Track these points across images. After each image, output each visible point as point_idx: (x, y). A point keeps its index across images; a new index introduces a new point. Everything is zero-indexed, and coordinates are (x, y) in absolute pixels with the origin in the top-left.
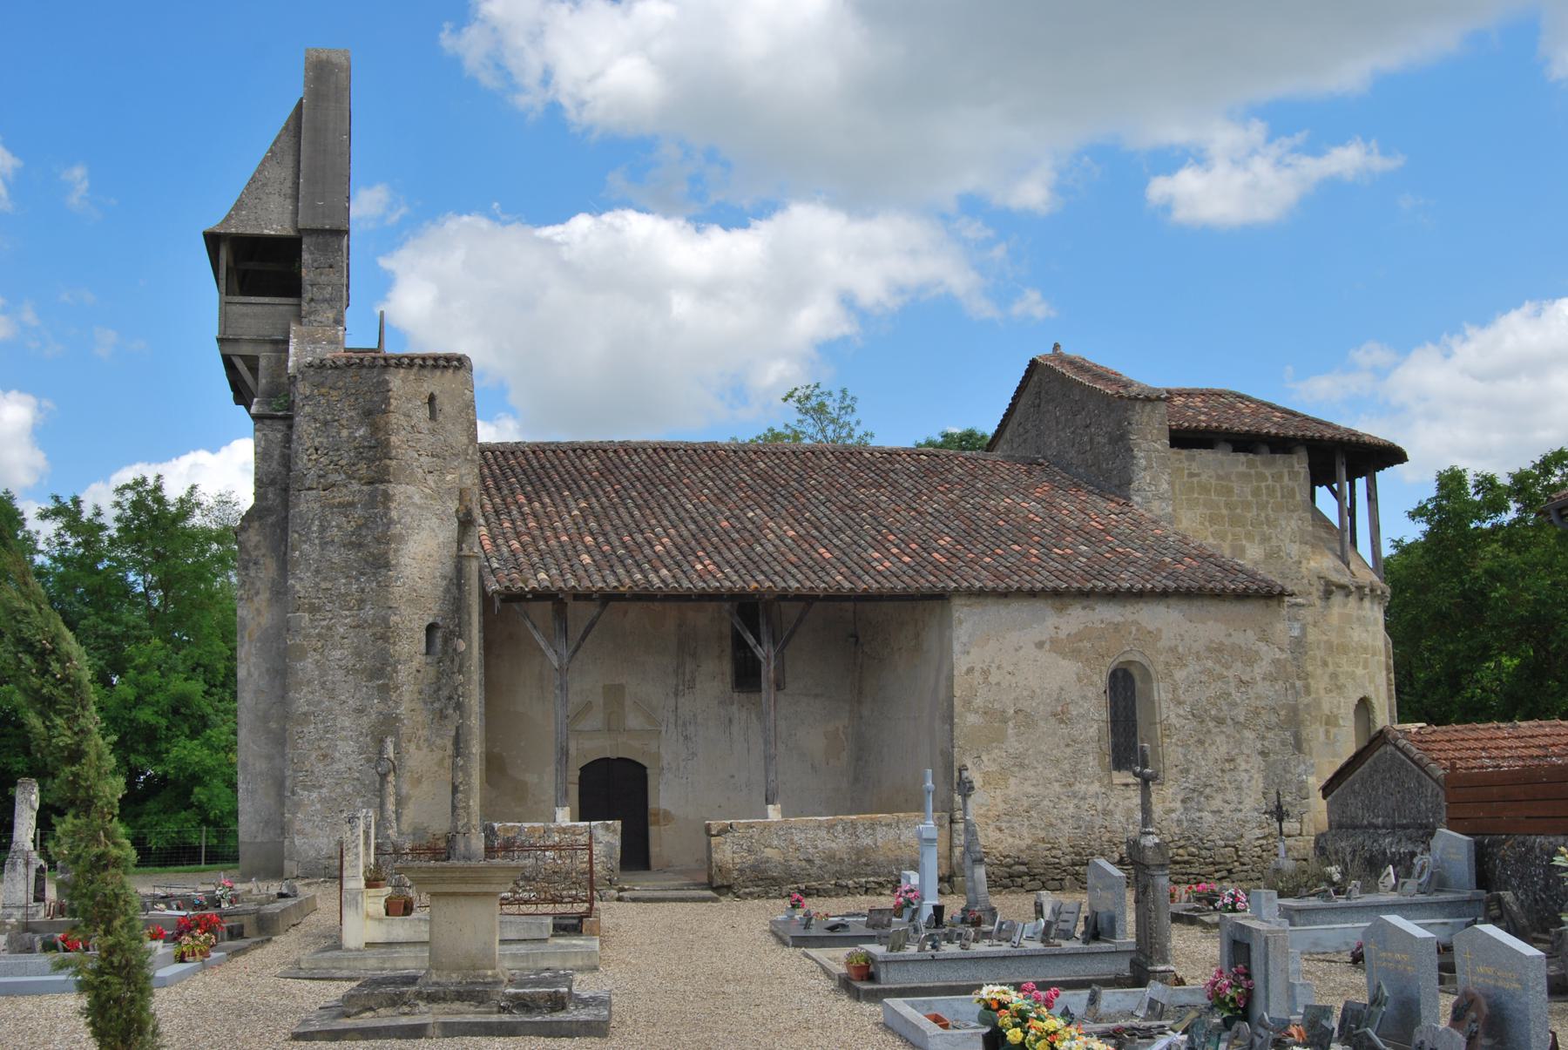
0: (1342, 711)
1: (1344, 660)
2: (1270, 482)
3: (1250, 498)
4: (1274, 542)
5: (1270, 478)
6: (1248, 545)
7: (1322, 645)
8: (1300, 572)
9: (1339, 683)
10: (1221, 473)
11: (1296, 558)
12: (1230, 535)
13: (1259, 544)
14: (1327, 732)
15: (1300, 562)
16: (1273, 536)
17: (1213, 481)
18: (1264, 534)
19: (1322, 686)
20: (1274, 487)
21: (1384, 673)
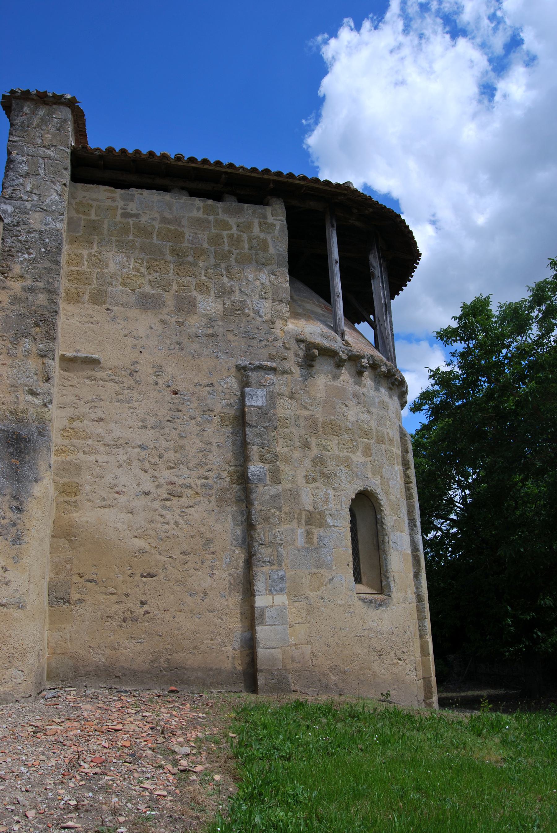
0: (331, 506)
1: (333, 443)
2: (234, 230)
3: (206, 245)
4: (237, 296)
5: (235, 228)
6: (200, 297)
7: (302, 422)
8: (271, 333)
9: (325, 470)
10: (168, 215)
11: (268, 317)
12: (175, 284)
13: (216, 298)
14: (308, 534)
15: (273, 323)
16: (237, 289)
17: (157, 224)
18: (223, 286)
19: (301, 473)
20: (239, 237)
21: (398, 468)
